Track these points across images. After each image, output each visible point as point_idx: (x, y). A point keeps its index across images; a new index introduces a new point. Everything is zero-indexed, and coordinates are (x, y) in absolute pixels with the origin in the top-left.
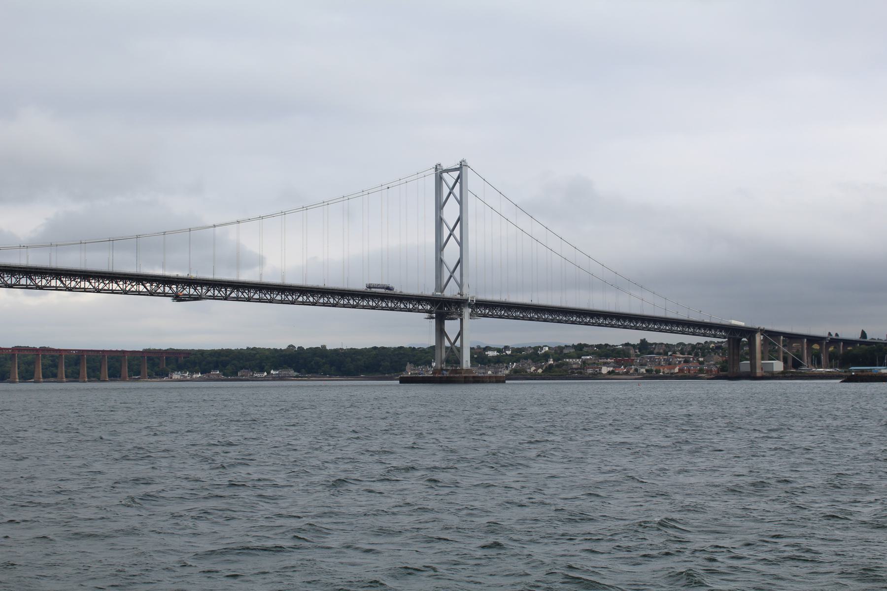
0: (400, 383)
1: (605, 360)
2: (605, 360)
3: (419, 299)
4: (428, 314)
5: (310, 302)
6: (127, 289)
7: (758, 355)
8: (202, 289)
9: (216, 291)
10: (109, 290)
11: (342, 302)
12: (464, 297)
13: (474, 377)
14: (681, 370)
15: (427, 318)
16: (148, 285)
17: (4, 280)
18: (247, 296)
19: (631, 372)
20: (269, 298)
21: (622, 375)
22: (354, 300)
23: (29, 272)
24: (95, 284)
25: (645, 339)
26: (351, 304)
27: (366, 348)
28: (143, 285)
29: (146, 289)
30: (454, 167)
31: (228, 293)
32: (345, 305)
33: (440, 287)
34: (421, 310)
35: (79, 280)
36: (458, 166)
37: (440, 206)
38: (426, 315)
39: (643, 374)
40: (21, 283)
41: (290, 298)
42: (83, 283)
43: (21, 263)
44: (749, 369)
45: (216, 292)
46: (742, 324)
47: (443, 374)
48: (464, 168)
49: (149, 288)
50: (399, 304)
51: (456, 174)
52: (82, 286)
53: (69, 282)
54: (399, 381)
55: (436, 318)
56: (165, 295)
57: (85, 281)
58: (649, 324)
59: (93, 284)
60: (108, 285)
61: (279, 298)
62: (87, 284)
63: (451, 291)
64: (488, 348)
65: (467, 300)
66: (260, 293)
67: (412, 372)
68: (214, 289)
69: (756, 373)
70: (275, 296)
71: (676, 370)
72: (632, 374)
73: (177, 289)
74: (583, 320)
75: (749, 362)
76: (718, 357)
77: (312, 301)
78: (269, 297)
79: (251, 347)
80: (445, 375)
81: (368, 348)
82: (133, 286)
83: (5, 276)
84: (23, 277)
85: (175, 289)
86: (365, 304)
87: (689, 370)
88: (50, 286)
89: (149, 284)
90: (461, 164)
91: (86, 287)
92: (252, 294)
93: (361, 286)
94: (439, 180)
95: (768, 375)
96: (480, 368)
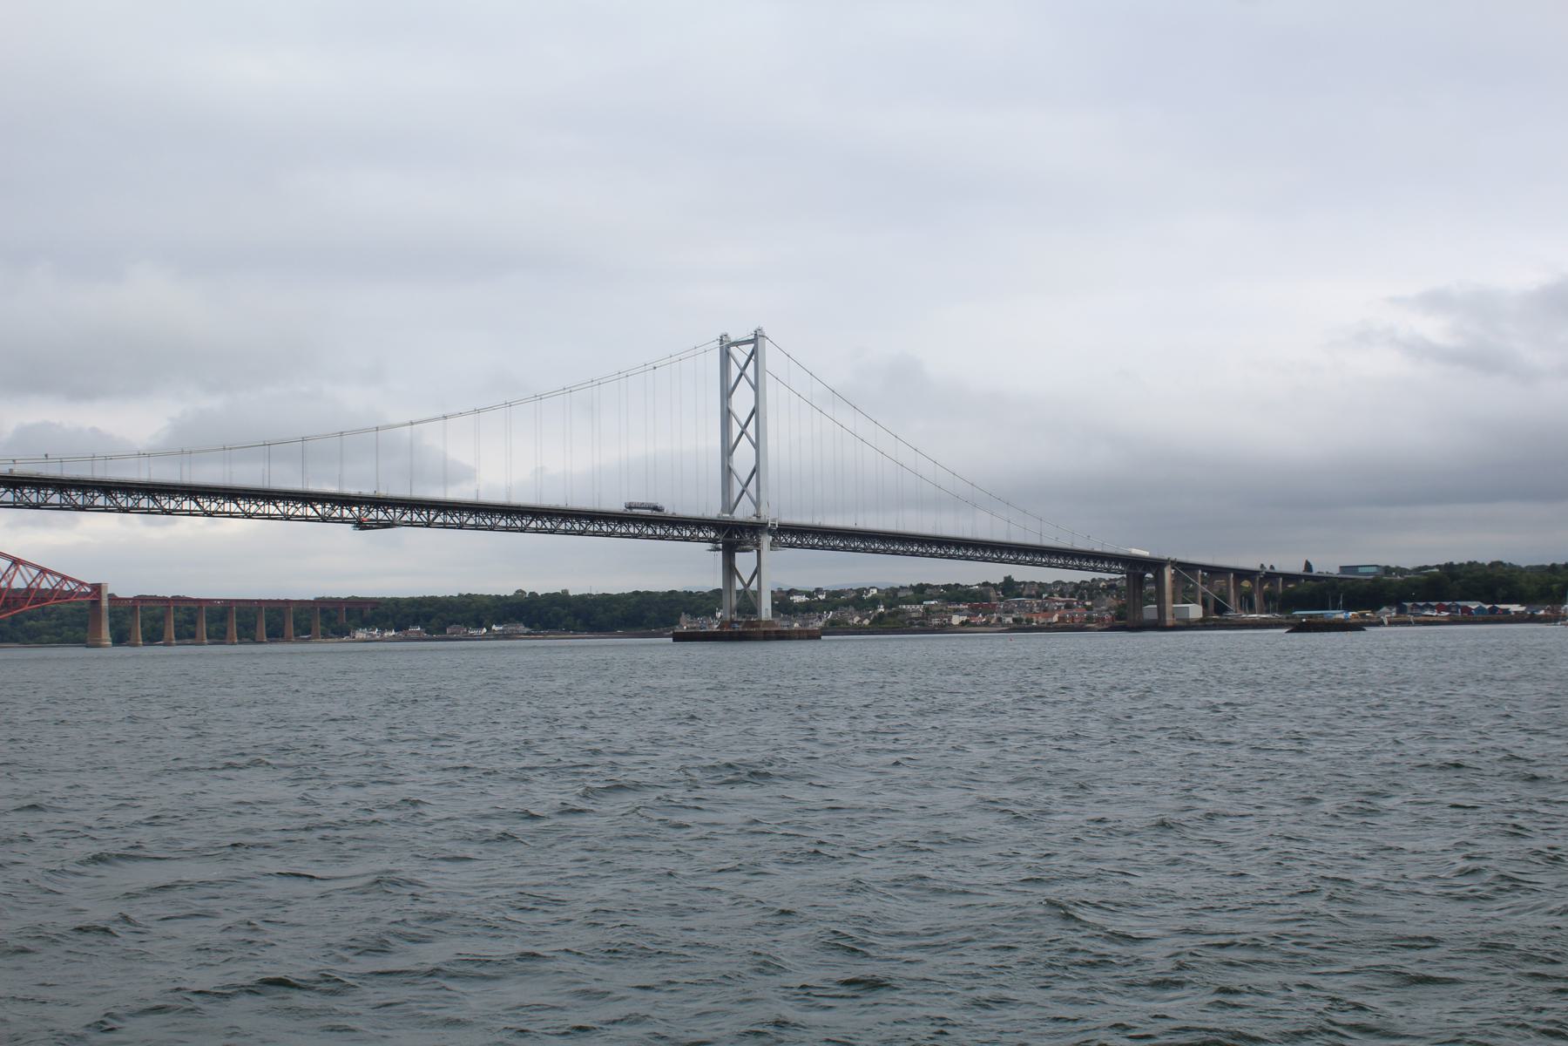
0: (674, 641)
1: (956, 607)
2: (956, 607)
3: (700, 523)
4: (711, 544)
5: (546, 528)
6: (290, 513)
7: (1168, 597)
8: (395, 512)
9: (414, 515)
10: (264, 514)
11: (591, 529)
12: (762, 520)
13: (777, 632)
14: (1061, 619)
15: (711, 550)
16: (319, 507)
17: (117, 502)
18: (458, 521)
19: (993, 622)
20: (489, 523)
21: (980, 626)
22: (608, 525)
23: (62, 485)
24: (245, 505)
25: (1010, 577)
26: (604, 532)
27: (385, 598)
28: (312, 506)
29: (317, 512)
30: (746, 339)
31: (432, 517)
32: (597, 532)
33: (729, 506)
34: (702, 538)
35: (262, 503)
36: (752, 337)
37: (727, 393)
38: (709, 546)
39: (1008, 624)
40: (141, 506)
41: (519, 523)
42: (227, 505)
43: (152, 477)
44: (1155, 616)
45: (415, 516)
46: (1145, 553)
47: (734, 628)
48: (760, 339)
49: (320, 511)
50: (644, 530)
51: (749, 348)
52: (227, 510)
53: (167, 501)
54: (671, 639)
55: (724, 550)
56: (343, 520)
57: (342, 508)
58: (1002, 554)
59: (242, 507)
60: (301, 509)
61: (503, 523)
62: (234, 506)
63: (744, 512)
64: (792, 592)
65: (767, 523)
66: (476, 516)
67: (689, 625)
68: (412, 512)
69: (1165, 621)
70: (497, 520)
71: (1055, 619)
72: (993, 625)
73: (360, 512)
74: (908, 550)
75: (1156, 606)
76: (1112, 600)
77: (549, 527)
78: (489, 523)
79: (465, 593)
80: (736, 629)
81: (1456, 563)
82: (298, 509)
83: (119, 495)
84: (143, 498)
85: (357, 513)
86: (623, 531)
87: (1073, 618)
88: (45, 503)
89: (357, 508)
90: (756, 335)
91: (232, 511)
92: (465, 518)
93: (616, 505)
94: (726, 356)
95: (1181, 623)
96: (784, 619)
